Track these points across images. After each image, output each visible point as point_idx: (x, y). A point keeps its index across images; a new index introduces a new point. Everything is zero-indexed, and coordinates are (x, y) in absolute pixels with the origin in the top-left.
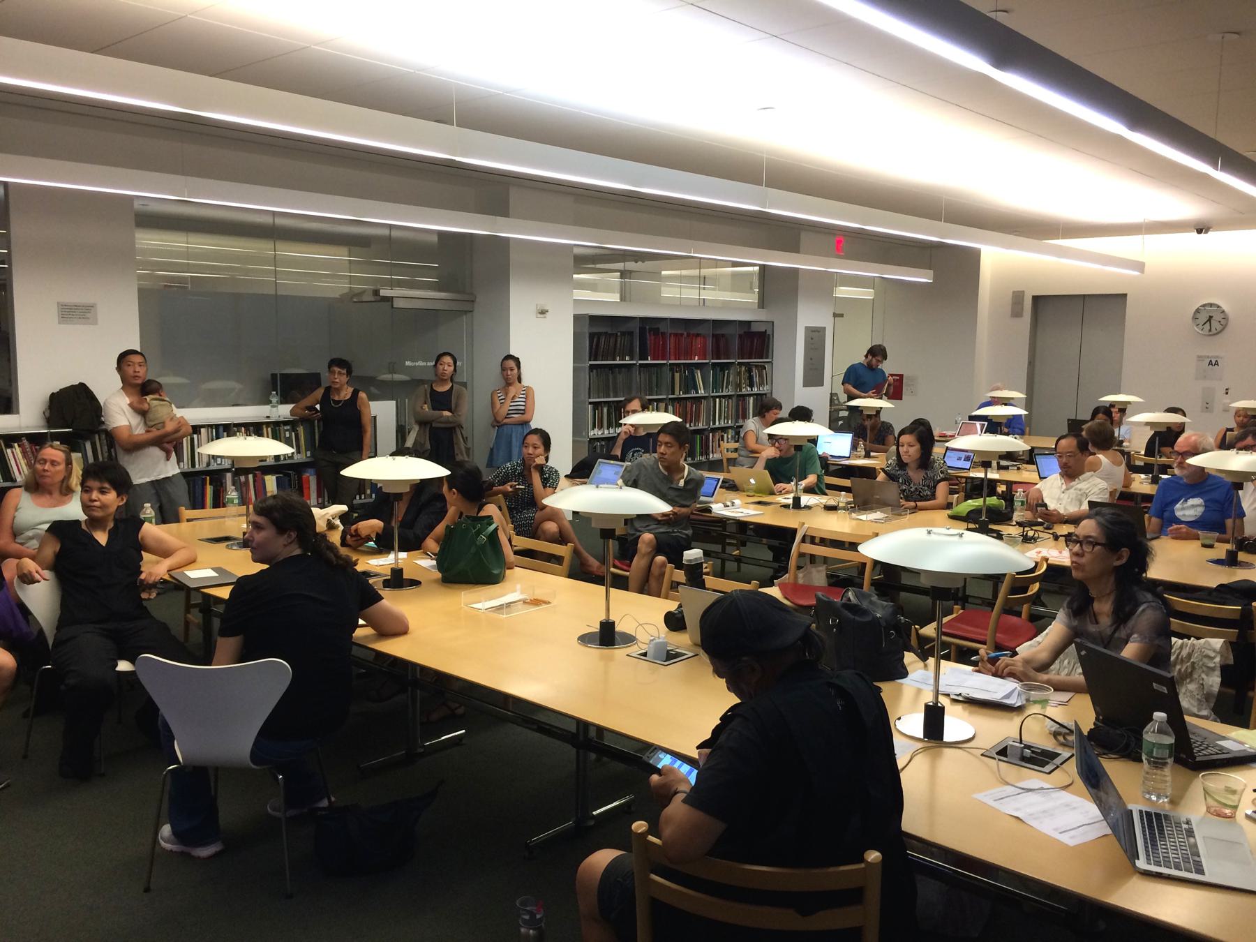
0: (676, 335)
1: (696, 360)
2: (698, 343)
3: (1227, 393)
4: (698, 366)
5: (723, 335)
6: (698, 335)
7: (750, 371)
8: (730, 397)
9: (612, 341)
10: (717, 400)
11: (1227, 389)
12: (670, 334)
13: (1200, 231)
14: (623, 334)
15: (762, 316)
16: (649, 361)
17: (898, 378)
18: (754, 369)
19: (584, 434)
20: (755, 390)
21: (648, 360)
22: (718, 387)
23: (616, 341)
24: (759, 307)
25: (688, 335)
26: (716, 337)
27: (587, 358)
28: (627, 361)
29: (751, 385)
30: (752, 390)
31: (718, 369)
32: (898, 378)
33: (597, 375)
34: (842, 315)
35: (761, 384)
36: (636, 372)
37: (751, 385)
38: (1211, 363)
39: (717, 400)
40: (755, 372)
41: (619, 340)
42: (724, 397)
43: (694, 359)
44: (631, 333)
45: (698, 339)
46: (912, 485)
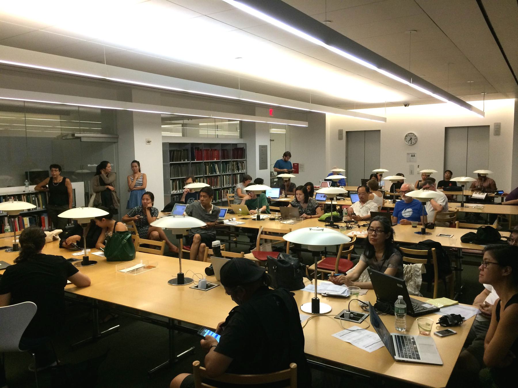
0: (206, 150)
1: (215, 160)
2: (216, 153)
3: (418, 167)
4: (216, 162)
5: (226, 150)
6: (215, 150)
7: (237, 164)
8: (230, 175)
9: (179, 153)
10: (225, 176)
11: (418, 165)
12: (204, 150)
13: (406, 106)
14: (184, 150)
15: (241, 141)
16: (196, 161)
17: (297, 165)
18: (239, 163)
19: (169, 192)
20: (240, 172)
21: (195, 161)
22: (225, 171)
23: (181, 153)
24: (240, 138)
25: (211, 150)
26: (223, 150)
27: (169, 161)
28: (186, 161)
29: (238, 170)
30: (239, 172)
31: (225, 164)
32: (297, 165)
33: (174, 168)
34: (273, 140)
35: (242, 169)
36: (190, 166)
37: (238, 170)
38: (412, 156)
39: (225, 176)
40: (240, 164)
41: (182, 153)
42: (227, 175)
43: (214, 160)
44: (187, 150)
45: (216, 151)
46: (303, 209)
